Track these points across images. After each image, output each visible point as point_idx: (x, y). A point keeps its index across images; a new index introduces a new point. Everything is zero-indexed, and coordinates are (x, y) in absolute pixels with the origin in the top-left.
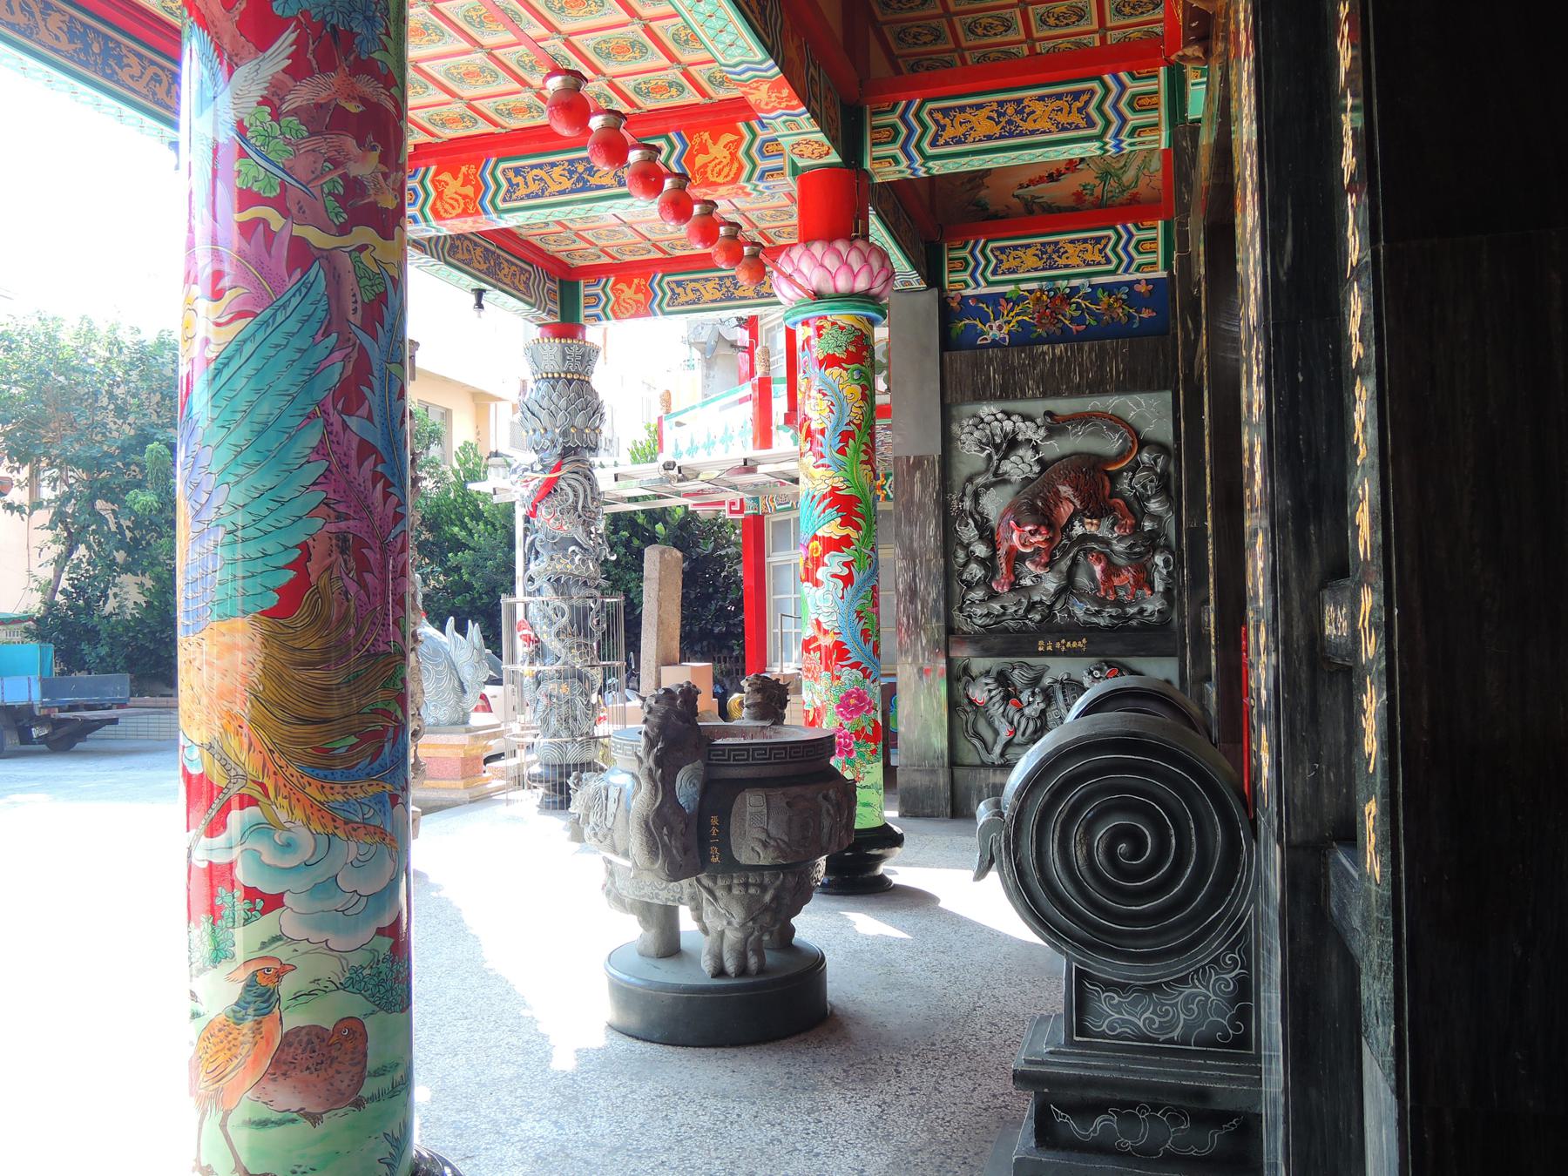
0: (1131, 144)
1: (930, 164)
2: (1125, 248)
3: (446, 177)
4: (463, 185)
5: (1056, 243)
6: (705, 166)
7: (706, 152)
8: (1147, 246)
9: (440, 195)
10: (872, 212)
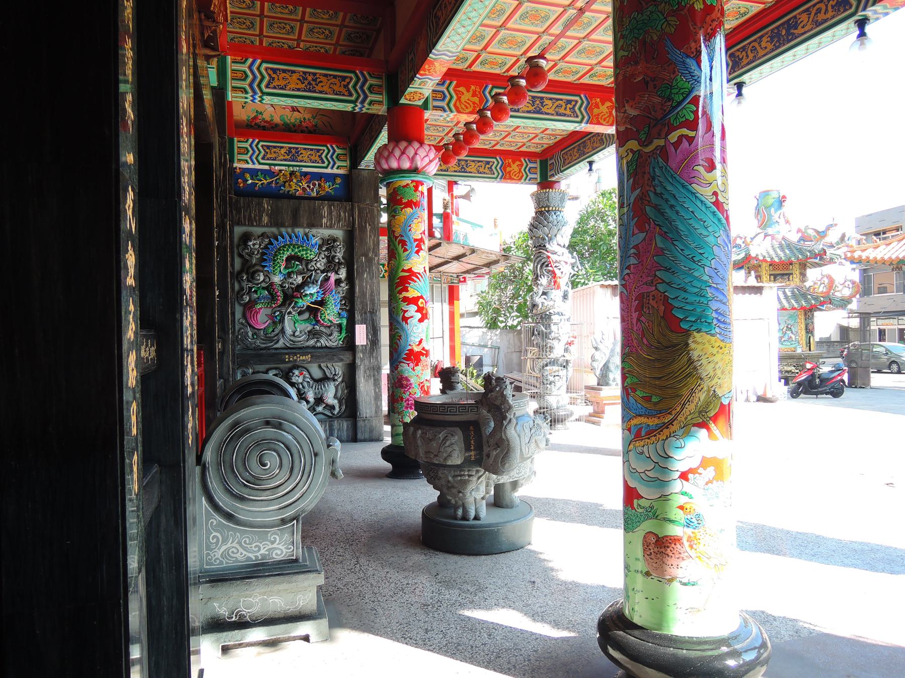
0: (246, 98)
1: (264, 97)
2: (331, 157)
3: (462, 89)
4: (473, 96)
5: (297, 148)
6: (598, 115)
7: (598, 108)
8: (533, 170)
9: (459, 98)
10: (386, 127)
